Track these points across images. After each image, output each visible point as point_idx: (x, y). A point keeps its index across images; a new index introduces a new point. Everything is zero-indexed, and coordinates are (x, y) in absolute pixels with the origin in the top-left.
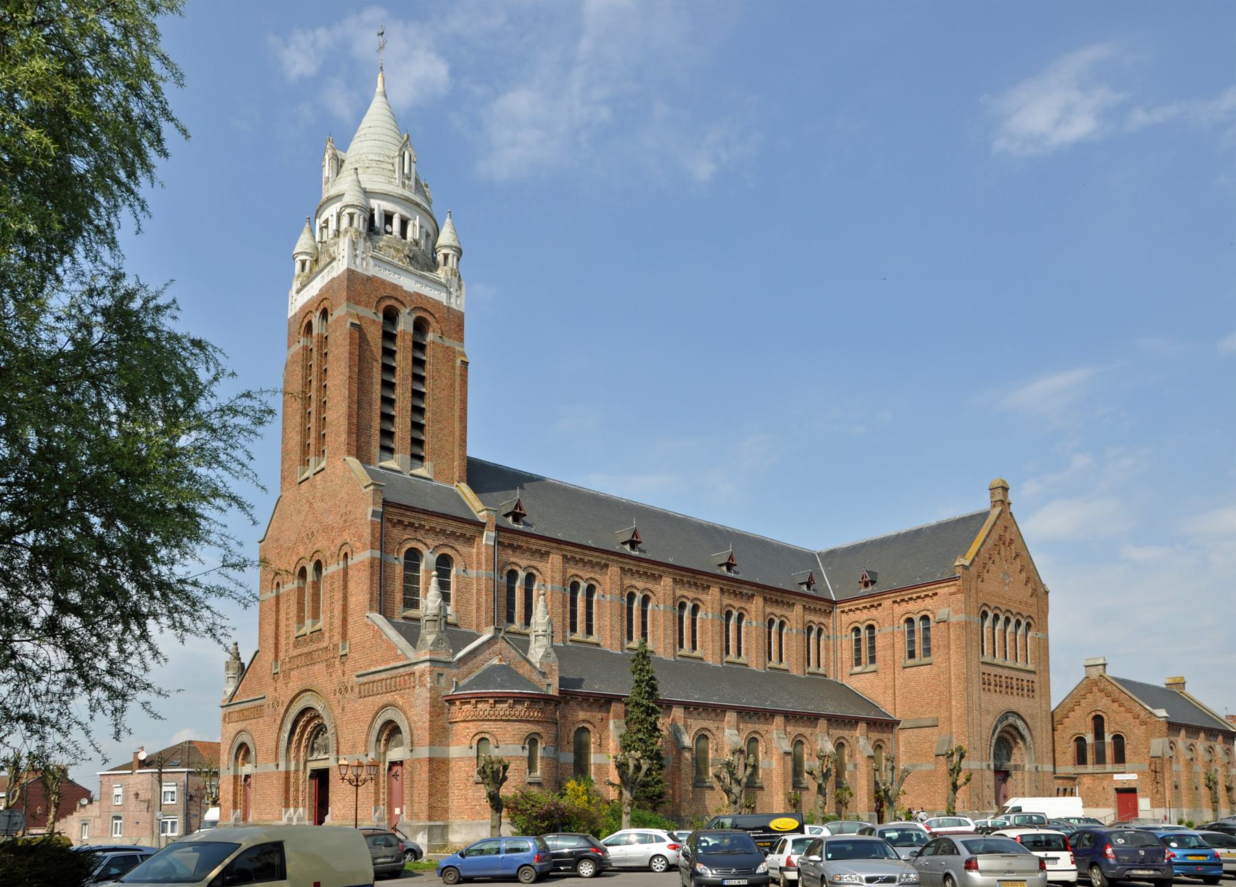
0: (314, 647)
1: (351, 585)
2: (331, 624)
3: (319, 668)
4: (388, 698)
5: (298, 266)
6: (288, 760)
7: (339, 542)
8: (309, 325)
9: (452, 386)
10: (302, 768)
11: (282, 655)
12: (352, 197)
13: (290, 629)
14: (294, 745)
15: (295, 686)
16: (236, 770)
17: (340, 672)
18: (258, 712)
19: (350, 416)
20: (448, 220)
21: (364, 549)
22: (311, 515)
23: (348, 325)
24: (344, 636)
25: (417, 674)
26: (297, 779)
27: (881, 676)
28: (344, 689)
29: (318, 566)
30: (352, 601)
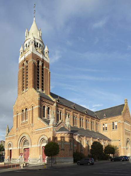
0: (25, 125)
1: (34, 113)
2: (29, 120)
3: (27, 129)
4: (43, 134)
5: (21, 53)
6: (20, 147)
7: (31, 104)
8: (24, 64)
9: (48, 77)
10: (22, 148)
11: (18, 127)
12: (32, 38)
13: (20, 121)
14: (21, 144)
15: (21, 132)
16: (8, 149)
17: (31, 129)
18: (13, 138)
19: (33, 80)
20: (46, 46)
21: (37, 105)
22: (24, 100)
23: (32, 63)
24: (32, 122)
25: (50, 129)
26: (21, 150)
27: (108, 132)
28: (32, 132)
29: (26, 109)
30: (34, 115)
